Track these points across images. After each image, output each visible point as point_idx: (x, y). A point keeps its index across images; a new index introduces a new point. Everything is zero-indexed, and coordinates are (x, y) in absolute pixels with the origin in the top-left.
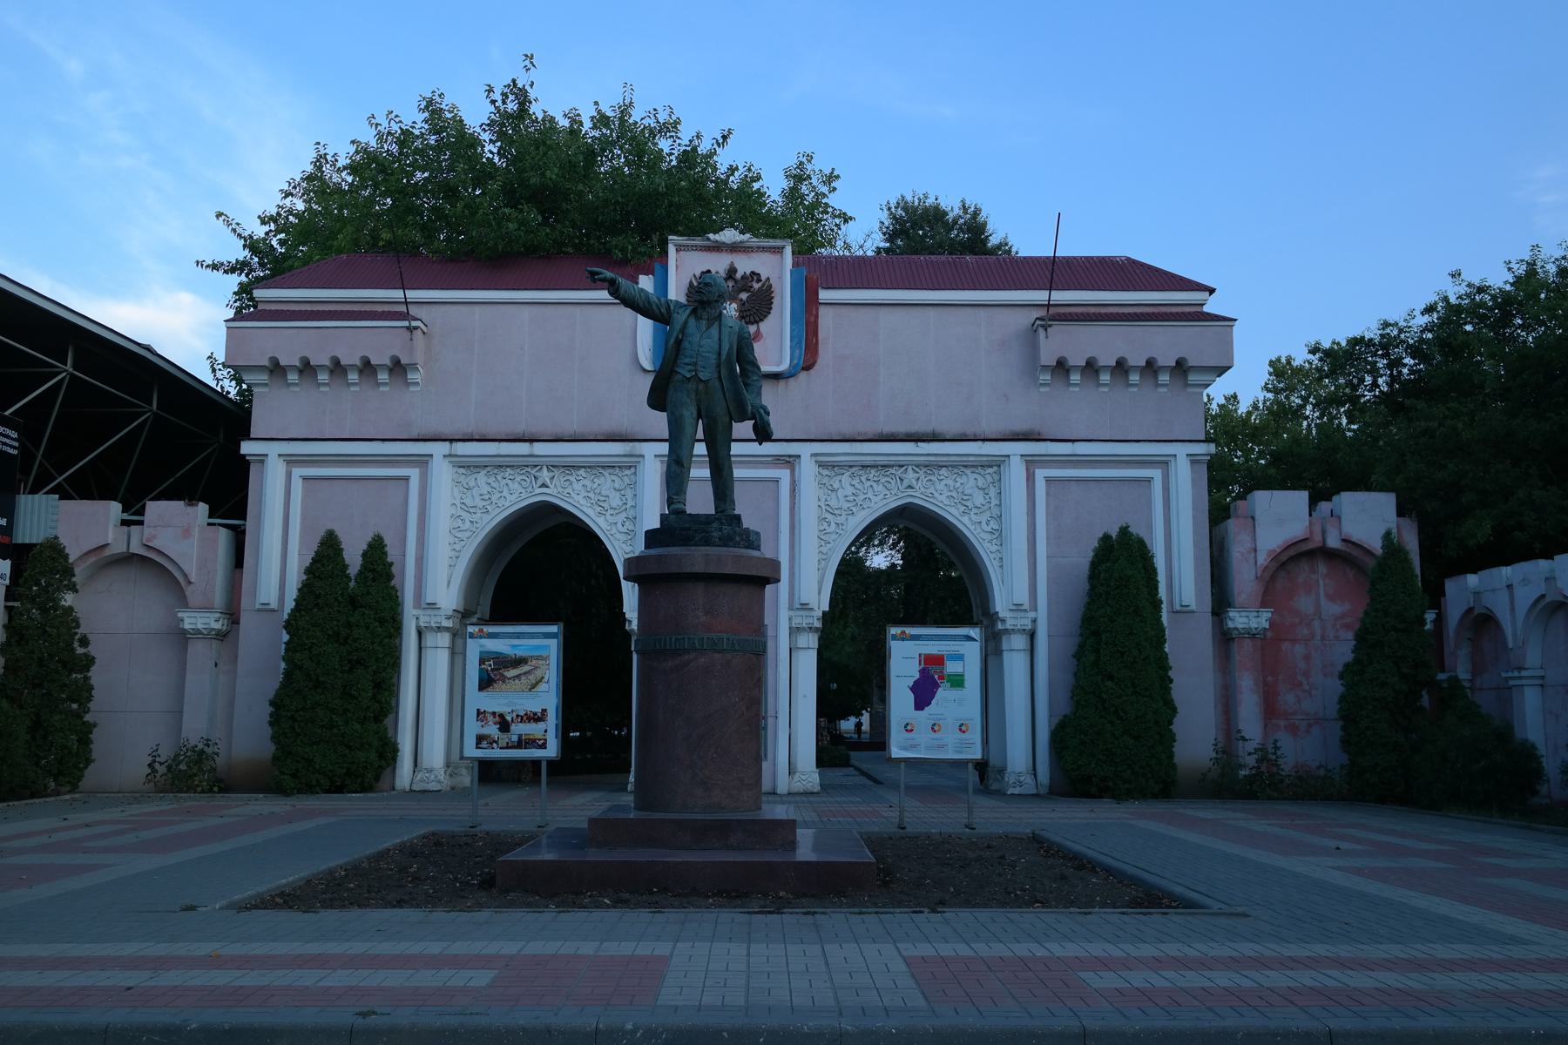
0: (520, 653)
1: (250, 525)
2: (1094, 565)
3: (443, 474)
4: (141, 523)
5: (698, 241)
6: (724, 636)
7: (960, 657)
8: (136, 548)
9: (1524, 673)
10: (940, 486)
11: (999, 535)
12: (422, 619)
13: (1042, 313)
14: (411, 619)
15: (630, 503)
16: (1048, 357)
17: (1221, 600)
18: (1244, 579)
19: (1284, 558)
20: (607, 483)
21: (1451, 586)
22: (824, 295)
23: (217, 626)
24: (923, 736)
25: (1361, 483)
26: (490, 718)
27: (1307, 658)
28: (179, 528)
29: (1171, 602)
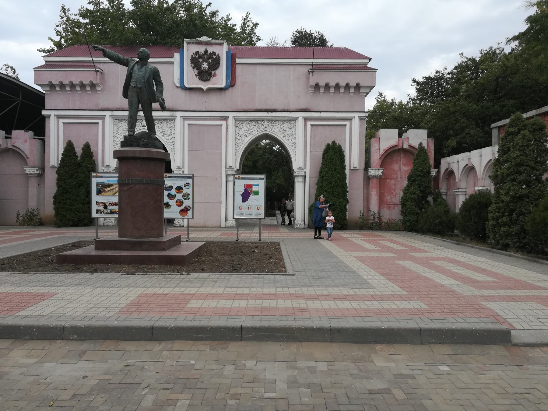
0: (110, 183)
1: (46, 138)
2: (324, 154)
3: (108, 121)
4: (10, 138)
5: (194, 41)
6: (145, 179)
7: (258, 185)
8: (10, 146)
9: (460, 190)
10: (276, 127)
11: (294, 143)
13: (311, 67)
15: (294, 133)
16: (313, 83)
17: (367, 165)
18: (375, 158)
19: (389, 152)
22: (237, 60)
23: (38, 172)
24: (245, 211)
25: (417, 127)
26: (101, 204)
27: (395, 184)
28: (22, 139)
29: (350, 166)
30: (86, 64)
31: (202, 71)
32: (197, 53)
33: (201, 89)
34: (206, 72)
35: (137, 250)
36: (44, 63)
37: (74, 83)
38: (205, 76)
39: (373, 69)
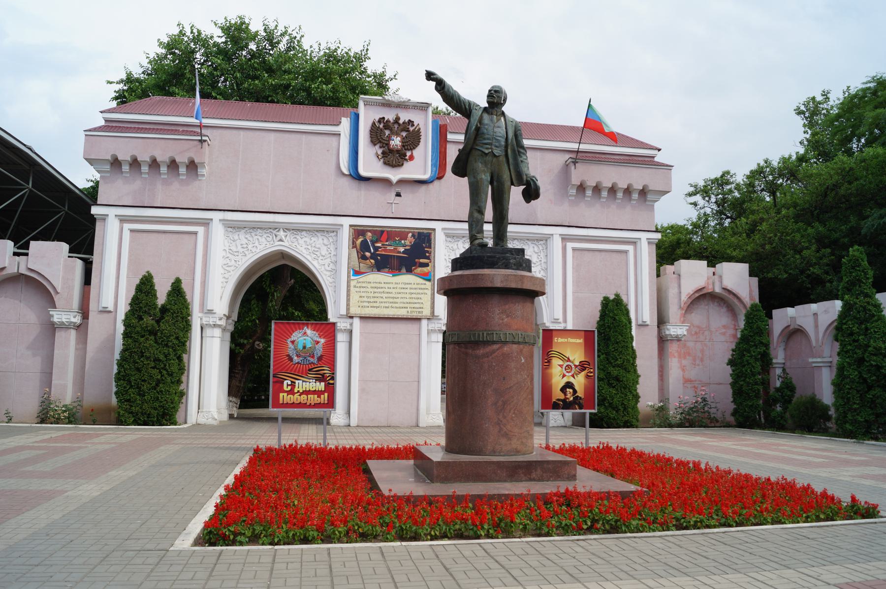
1: (95, 258)
3: (218, 229)
4: (27, 254)
8: (23, 270)
10: (301, 241)
12: (204, 319)
13: (573, 156)
14: (197, 319)
16: (575, 180)
20: (319, 241)
21: (775, 312)
25: (730, 259)
28: (50, 258)
30: (181, 129)
31: (391, 151)
32: (381, 120)
33: (386, 182)
34: (398, 151)
35: (521, 481)
36: (103, 123)
37: (119, 159)
38: (394, 158)
39: (667, 166)
